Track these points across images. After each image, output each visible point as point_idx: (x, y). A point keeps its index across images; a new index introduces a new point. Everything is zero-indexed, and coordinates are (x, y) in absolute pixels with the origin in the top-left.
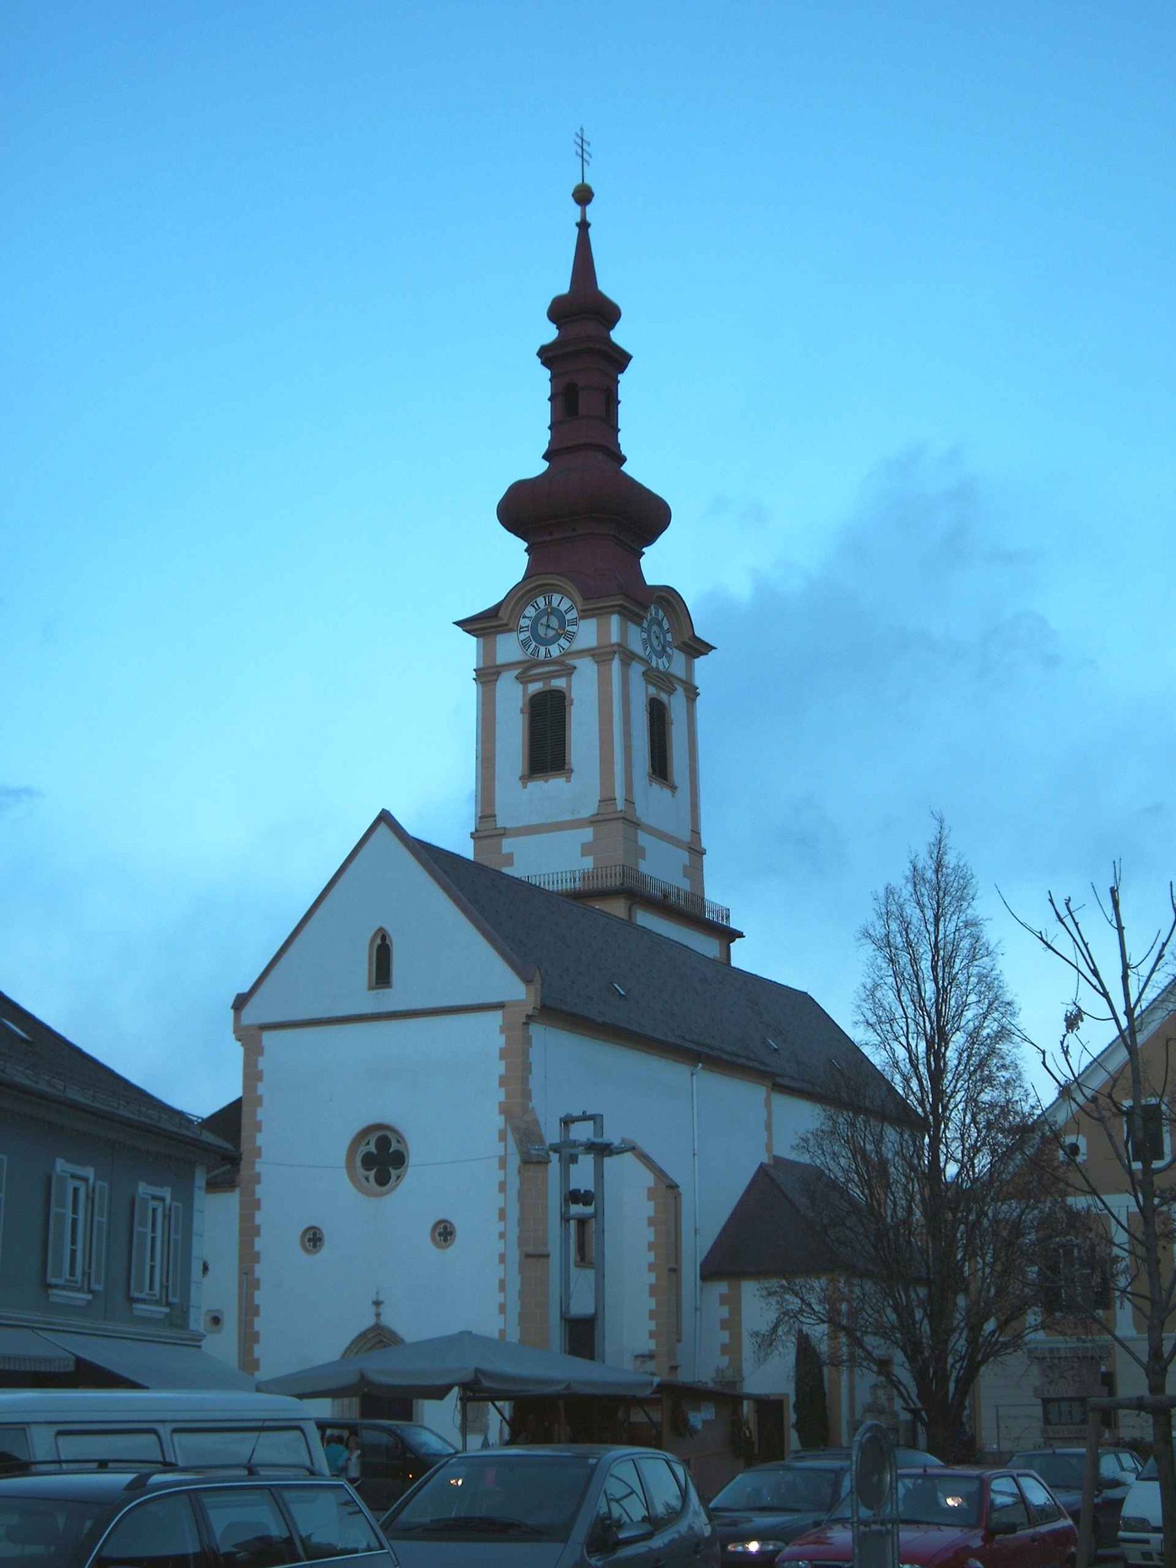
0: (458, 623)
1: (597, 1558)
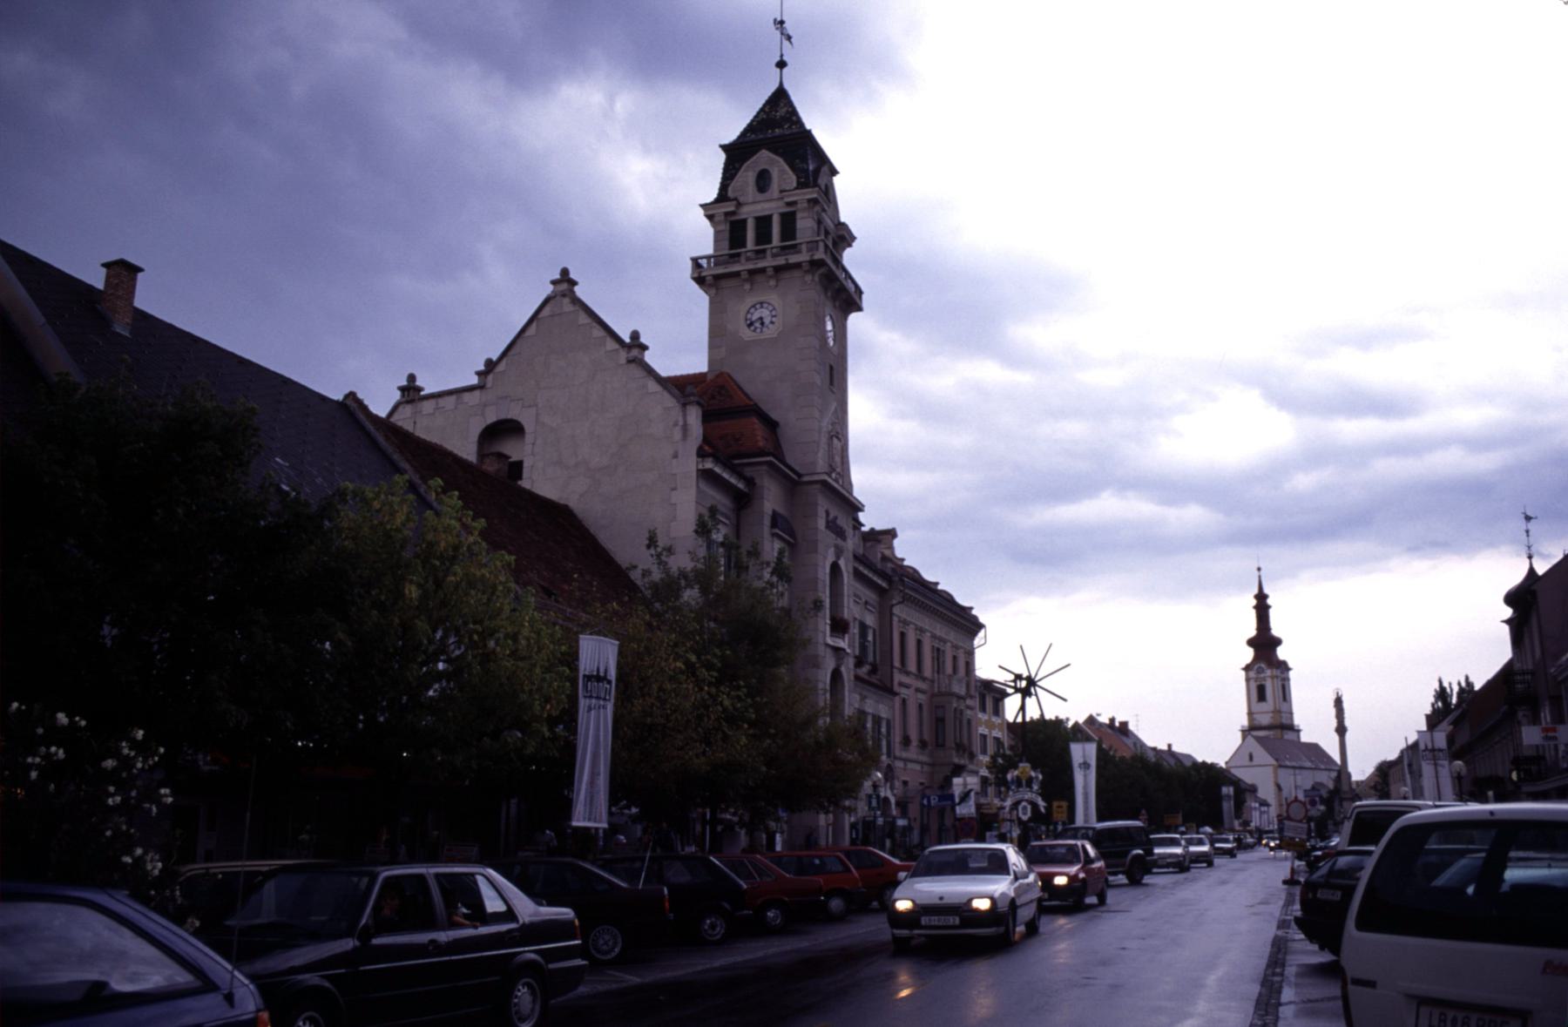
1: (1006, 742)
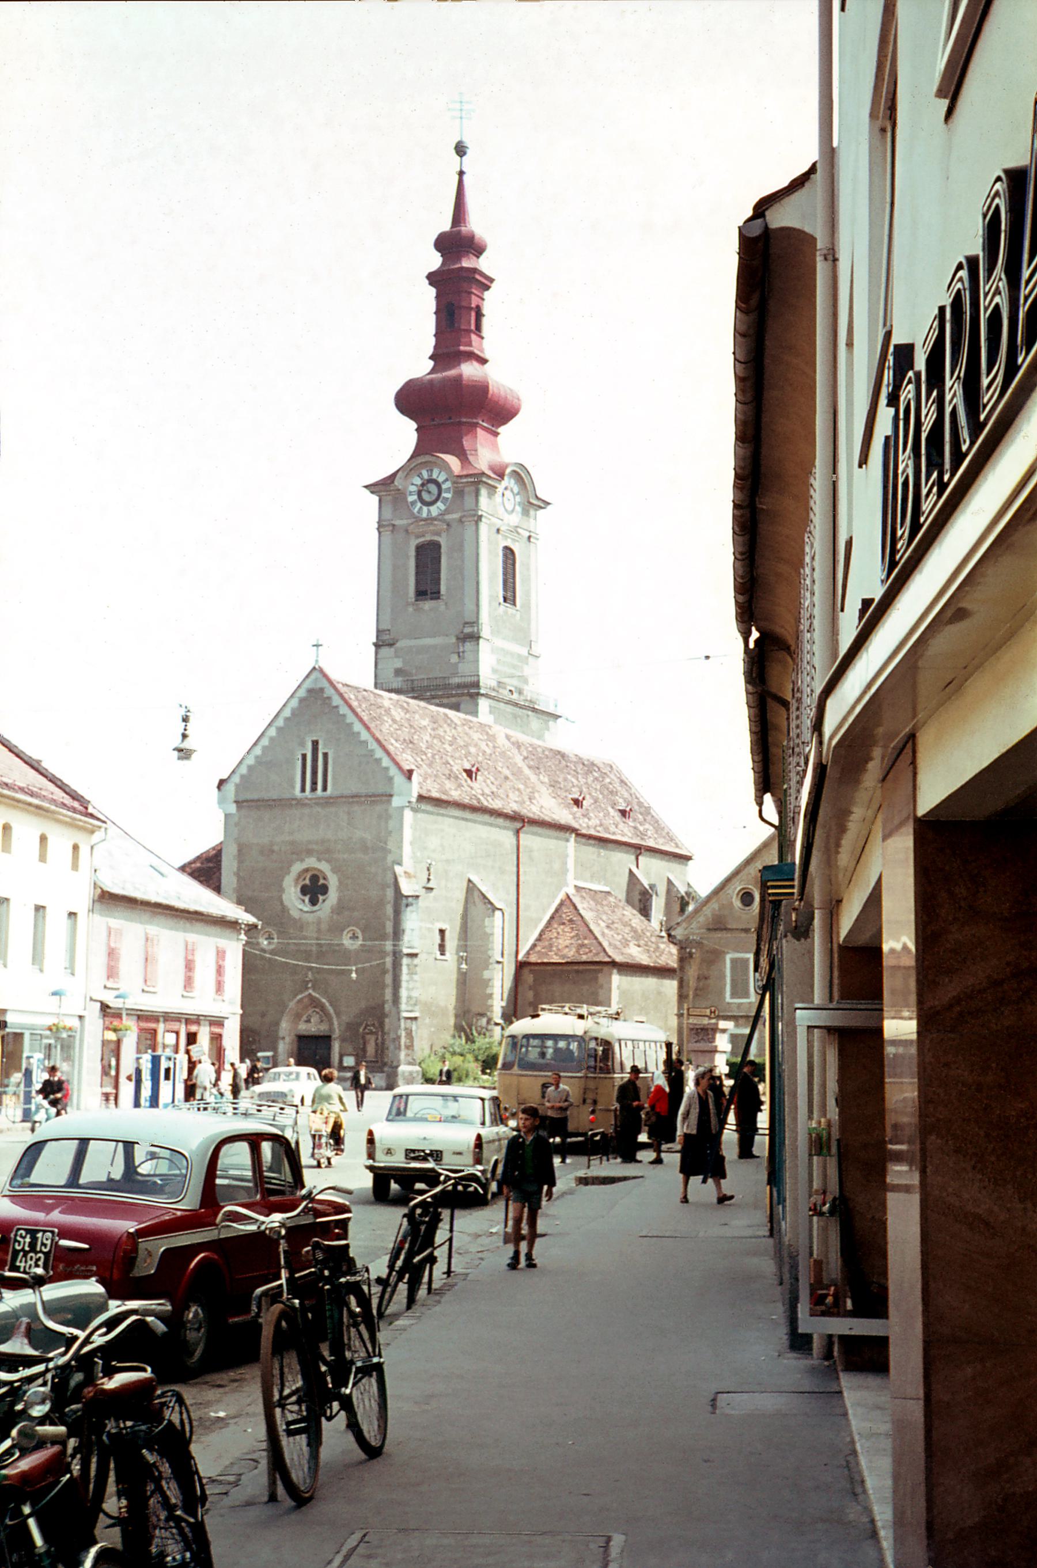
0: (366, 487)
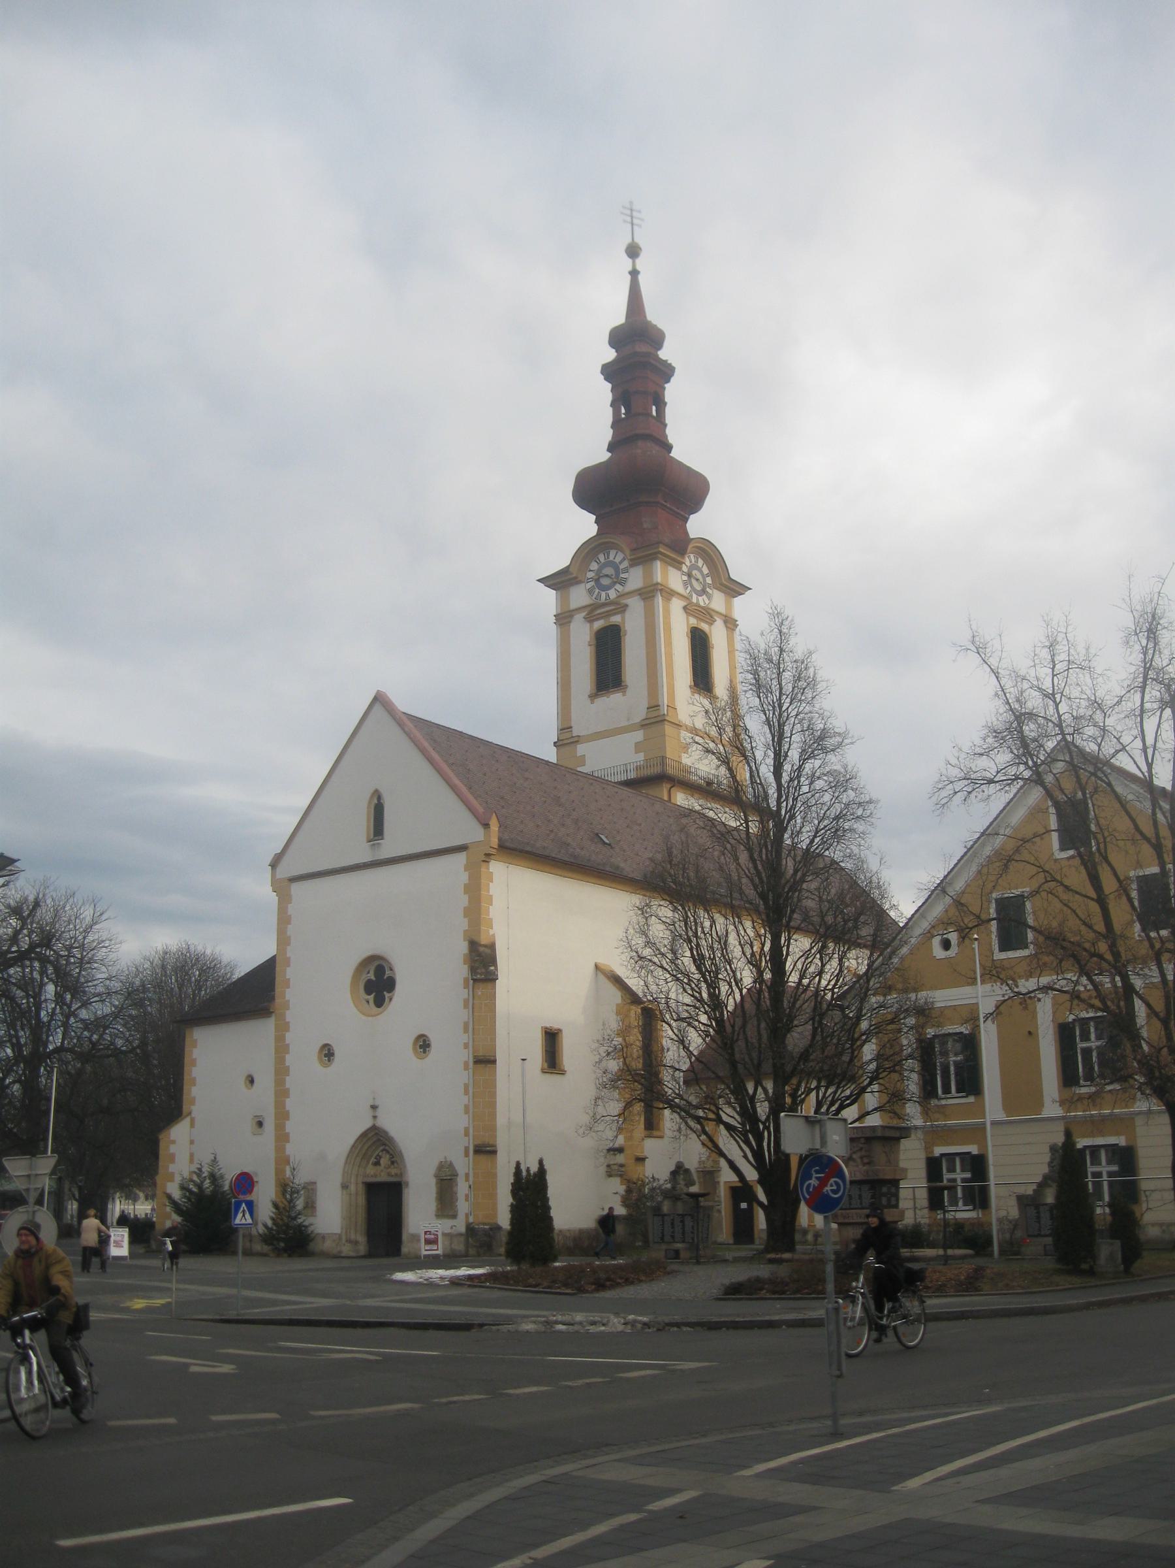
0: (538, 580)
